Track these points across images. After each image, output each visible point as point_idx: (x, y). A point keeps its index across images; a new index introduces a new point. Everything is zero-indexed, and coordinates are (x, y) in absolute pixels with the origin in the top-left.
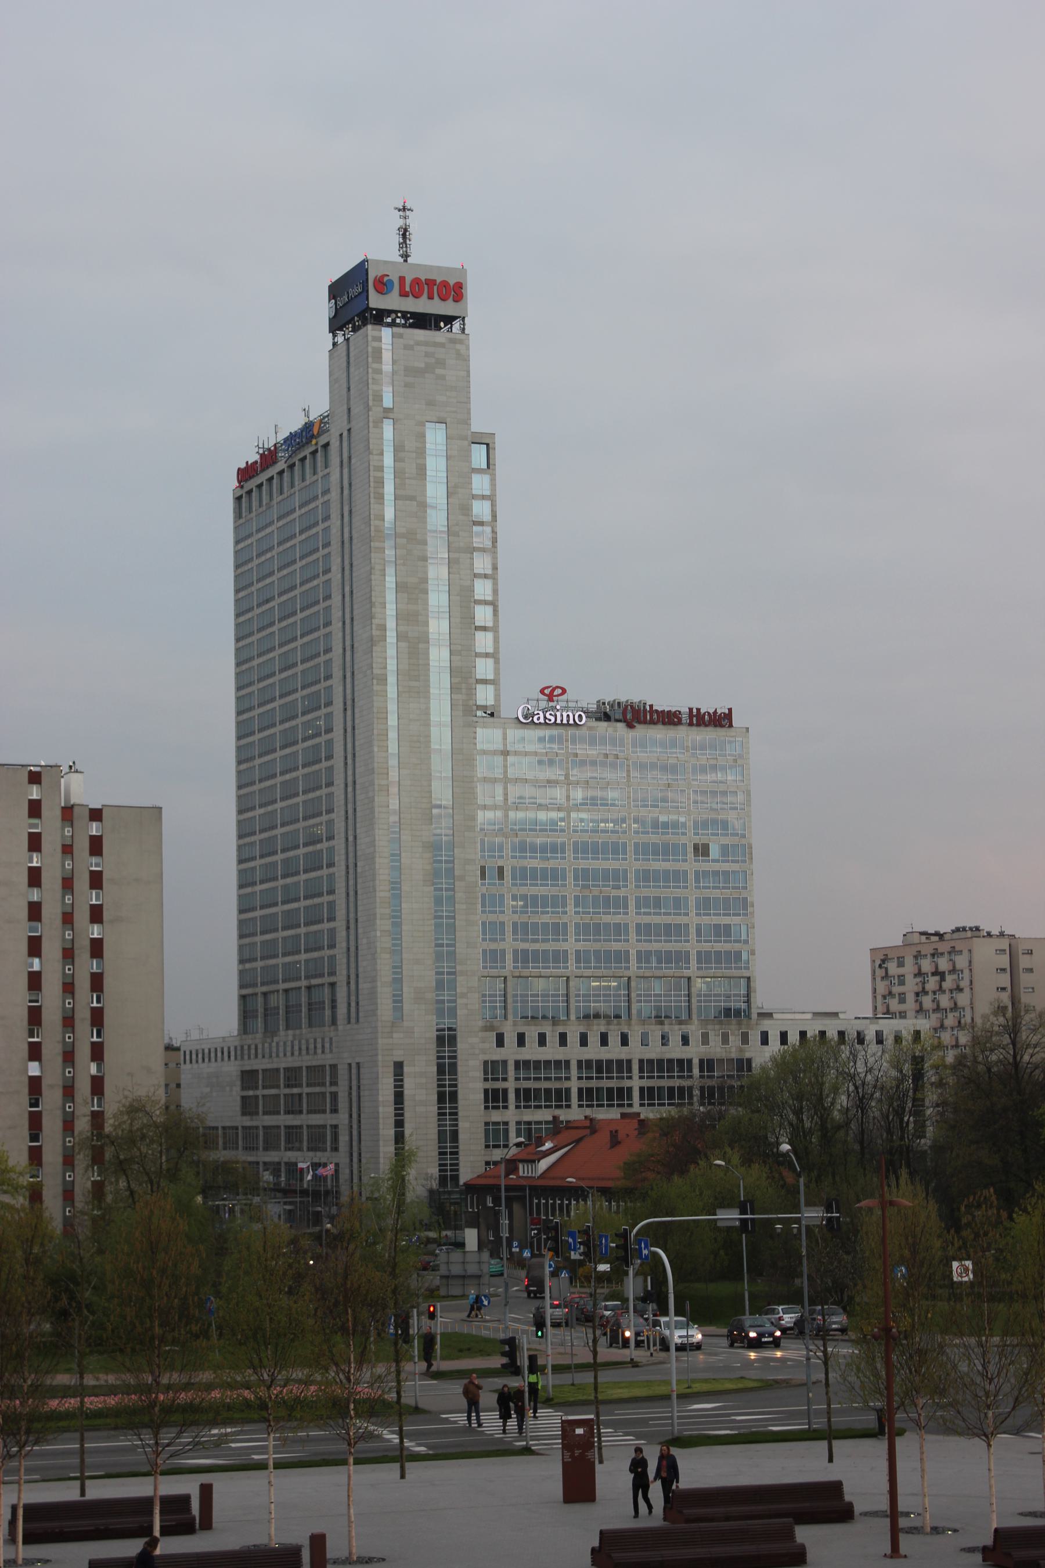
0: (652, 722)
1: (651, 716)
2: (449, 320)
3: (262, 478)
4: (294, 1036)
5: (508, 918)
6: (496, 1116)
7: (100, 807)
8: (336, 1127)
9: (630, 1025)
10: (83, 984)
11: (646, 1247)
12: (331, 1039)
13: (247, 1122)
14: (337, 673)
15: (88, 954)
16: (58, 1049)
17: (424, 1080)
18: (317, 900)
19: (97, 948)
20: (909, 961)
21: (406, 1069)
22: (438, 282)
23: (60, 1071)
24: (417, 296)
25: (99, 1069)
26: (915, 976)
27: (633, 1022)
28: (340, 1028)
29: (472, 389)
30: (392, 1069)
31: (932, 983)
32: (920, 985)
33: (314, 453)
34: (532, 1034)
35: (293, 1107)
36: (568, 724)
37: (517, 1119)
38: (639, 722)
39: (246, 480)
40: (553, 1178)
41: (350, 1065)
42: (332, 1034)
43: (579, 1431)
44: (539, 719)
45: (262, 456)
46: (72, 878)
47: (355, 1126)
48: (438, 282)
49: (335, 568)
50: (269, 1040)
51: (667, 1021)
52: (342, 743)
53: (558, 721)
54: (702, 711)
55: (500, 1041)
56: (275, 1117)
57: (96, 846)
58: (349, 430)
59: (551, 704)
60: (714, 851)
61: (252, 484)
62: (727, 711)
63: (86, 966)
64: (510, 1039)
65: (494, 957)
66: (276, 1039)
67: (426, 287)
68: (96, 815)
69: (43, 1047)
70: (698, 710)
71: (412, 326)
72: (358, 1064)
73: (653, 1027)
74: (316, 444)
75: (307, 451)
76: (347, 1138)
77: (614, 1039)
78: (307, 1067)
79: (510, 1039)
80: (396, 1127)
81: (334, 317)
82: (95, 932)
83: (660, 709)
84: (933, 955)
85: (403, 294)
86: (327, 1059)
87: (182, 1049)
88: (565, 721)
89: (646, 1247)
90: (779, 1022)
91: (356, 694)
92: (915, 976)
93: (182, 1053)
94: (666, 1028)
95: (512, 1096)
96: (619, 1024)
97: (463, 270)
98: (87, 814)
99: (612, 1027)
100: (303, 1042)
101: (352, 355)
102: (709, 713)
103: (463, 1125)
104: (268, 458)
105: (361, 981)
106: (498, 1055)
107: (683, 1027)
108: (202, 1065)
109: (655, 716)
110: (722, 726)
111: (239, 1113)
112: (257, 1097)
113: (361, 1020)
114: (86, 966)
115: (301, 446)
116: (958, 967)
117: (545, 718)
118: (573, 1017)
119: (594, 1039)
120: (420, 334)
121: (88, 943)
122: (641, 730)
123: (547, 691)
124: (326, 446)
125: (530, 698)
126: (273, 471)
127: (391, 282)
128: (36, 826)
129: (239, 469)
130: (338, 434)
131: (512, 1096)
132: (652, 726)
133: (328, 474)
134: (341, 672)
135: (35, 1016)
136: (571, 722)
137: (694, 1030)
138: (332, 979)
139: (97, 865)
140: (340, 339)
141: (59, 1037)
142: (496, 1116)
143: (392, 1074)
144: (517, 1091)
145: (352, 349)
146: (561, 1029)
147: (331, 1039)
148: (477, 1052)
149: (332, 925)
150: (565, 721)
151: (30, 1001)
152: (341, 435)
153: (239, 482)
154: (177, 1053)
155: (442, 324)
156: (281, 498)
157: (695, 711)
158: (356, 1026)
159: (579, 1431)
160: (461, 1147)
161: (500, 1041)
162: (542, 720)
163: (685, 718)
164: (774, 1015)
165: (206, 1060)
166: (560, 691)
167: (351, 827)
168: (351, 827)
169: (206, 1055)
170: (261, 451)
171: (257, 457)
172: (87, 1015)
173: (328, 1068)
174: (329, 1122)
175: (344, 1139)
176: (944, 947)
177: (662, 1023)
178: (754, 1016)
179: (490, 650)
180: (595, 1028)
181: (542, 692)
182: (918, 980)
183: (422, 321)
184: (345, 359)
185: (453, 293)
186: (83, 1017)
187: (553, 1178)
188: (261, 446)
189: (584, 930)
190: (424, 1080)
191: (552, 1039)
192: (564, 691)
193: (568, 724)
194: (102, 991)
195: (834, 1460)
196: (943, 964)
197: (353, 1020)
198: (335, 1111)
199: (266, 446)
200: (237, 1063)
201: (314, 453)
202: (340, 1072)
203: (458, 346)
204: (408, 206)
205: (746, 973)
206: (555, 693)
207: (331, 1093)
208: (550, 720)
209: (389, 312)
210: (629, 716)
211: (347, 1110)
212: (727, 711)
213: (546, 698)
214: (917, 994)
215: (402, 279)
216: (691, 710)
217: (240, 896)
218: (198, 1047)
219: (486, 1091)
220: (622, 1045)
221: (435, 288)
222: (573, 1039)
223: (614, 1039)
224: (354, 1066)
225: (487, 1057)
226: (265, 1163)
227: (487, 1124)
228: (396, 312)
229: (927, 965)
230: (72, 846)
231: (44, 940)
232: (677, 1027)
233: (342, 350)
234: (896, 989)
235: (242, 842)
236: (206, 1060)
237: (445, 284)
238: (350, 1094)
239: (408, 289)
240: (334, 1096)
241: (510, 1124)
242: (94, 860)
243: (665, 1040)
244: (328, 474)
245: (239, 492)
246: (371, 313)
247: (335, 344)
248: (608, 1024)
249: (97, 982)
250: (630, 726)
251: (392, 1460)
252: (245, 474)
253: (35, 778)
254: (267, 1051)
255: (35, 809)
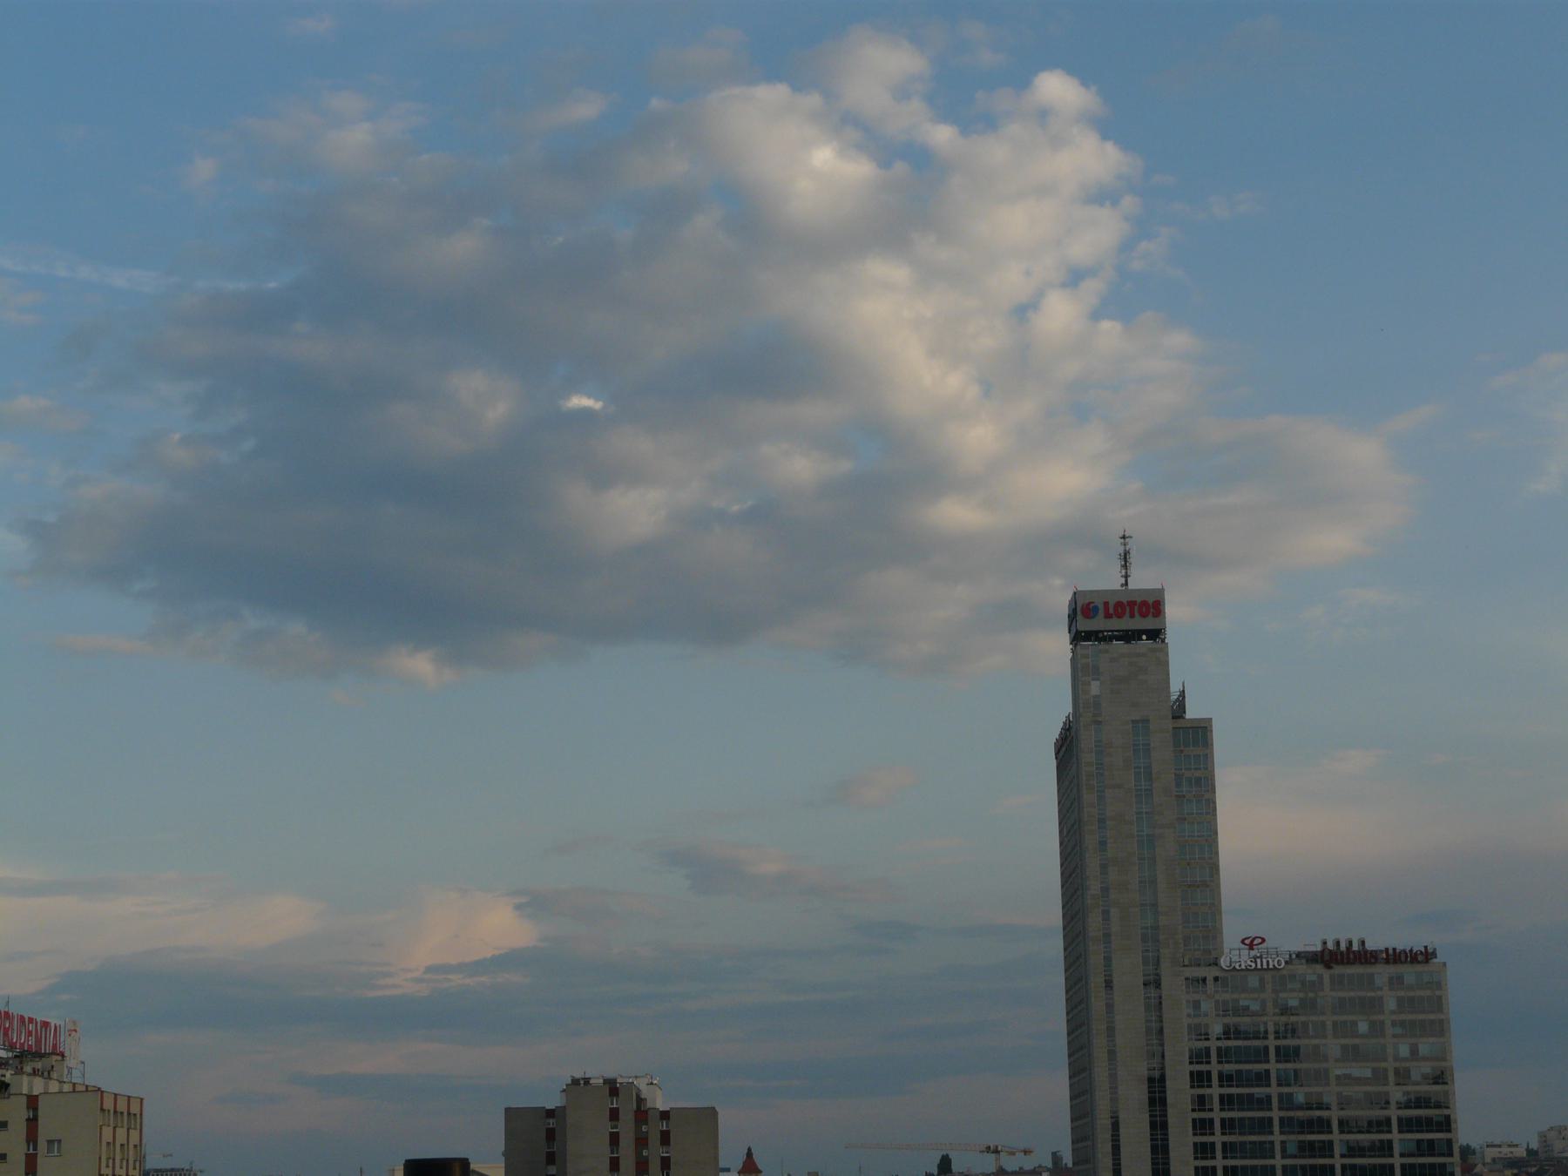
7: (668, 1109)
24: (1120, 616)
36: (1268, 969)
44: (1240, 966)
53: (1259, 966)
68: (665, 1115)
85: (1108, 616)
88: (1265, 966)
98: (658, 1114)
123: (1247, 942)
127: (1096, 608)
150: (1265, 966)
166: (1260, 940)
179: (77, 1090)
181: (1243, 942)
183: (1129, 636)
185: (1152, 610)
192: (1263, 940)
195: (727, 1166)
206: (1255, 942)
208: (1251, 966)
221: (1136, 608)
237: (1144, 603)
239: (1111, 611)
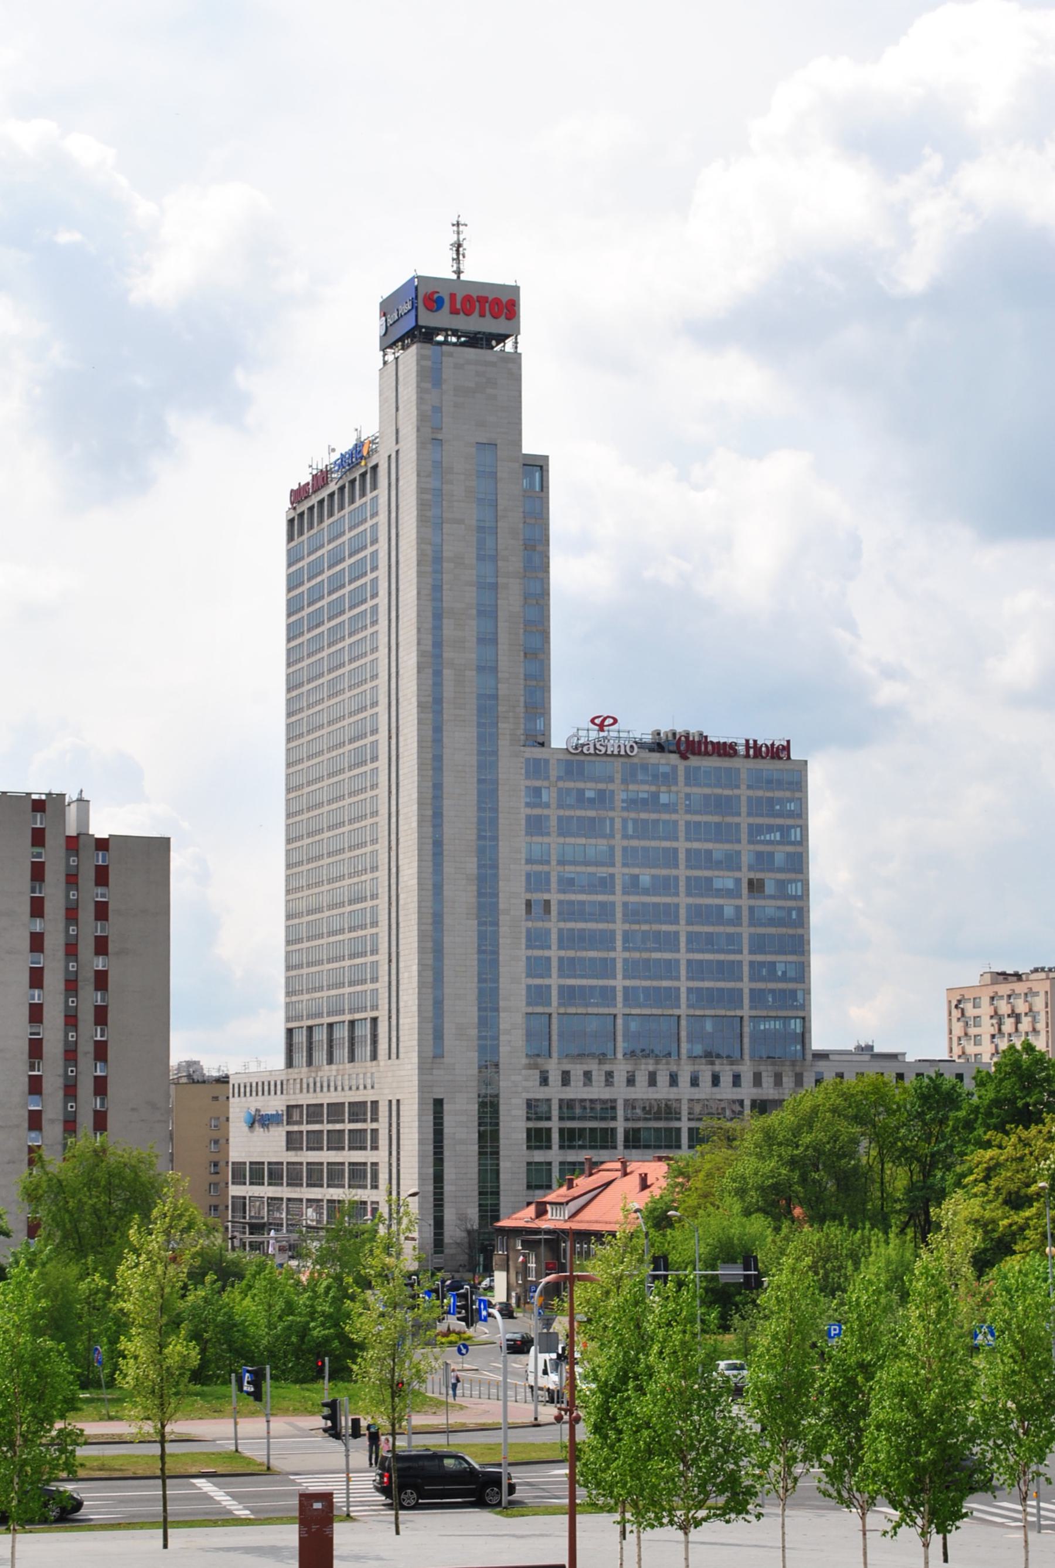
0: (707, 754)
1: (706, 748)
2: (502, 338)
3: (314, 500)
4: (338, 1070)
5: (554, 953)
6: (539, 1156)
8: (375, 1164)
9: (679, 1065)
10: (86, 1016)
11: (485, 1308)
12: (372, 1074)
13: (292, 1157)
14: (383, 700)
15: (92, 987)
16: (60, 1082)
17: (464, 1118)
18: (361, 933)
19: (101, 980)
20: (985, 1001)
21: (446, 1107)
22: (490, 299)
23: (60, 1105)
24: (468, 313)
25: (102, 1104)
26: (992, 1017)
27: (683, 1062)
28: (382, 1063)
29: (378, 421)
30: (431, 1107)
31: (1008, 1025)
32: (996, 1026)
33: (363, 475)
34: (577, 1071)
35: (335, 1141)
37: (561, 1159)
38: (694, 754)
39: (299, 502)
40: (581, 1222)
41: (390, 1101)
42: (374, 1070)
43: (317, 1506)
45: (315, 477)
46: (77, 908)
47: (394, 1164)
48: (490, 299)
49: (383, 592)
50: (313, 1075)
51: (717, 1061)
52: (387, 771)
54: (759, 743)
55: (544, 1081)
56: (339, 1153)
57: (102, 876)
58: (397, 452)
59: (602, 734)
60: (770, 888)
61: (304, 507)
62: (785, 744)
63: (89, 998)
64: (555, 1078)
65: (538, 995)
66: (320, 1074)
67: (477, 304)
69: (44, 1080)
70: (755, 741)
71: (462, 344)
72: (398, 1101)
73: (703, 1067)
74: (366, 465)
75: (357, 474)
76: (387, 1176)
77: (663, 1079)
78: (350, 1103)
79: (555, 1078)
80: (435, 1165)
81: (385, 334)
82: (100, 963)
83: (715, 740)
84: (1009, 996)
85: (454, 311)
86: (368, 1096)
87: (231, 1082)
89: (485, 1308)
90: (836, 1064)
91: (401, 722)
92: (992, 1017)
93: (231, 1086)
94: (717, 1068)
95: (555, 1136)
96: (668, 1063)
97: (516, 289)
99: (660, 1067)
100: (346, 1077)
101: (400, 374)
102: (766, 746)
103: (504, 1165)
104: (321, 479)
105: (401, 1015)
106: (541, 1093)
107: (734, 1067)
108: (250, 1099)
109: (710, 747)
110: (780, 758)
111: (285, 1148)
112: (301, 1132)
113: (401, 1055)
114: (89, 998)
115: (353, 466)
116: (1035, 1009)
117: (595, 748)
118: (620, 1056)
119: (642, 1079)
120: (471, 352)
121: (92, 975)
122: (694, 761)
123: (597, 721)
124: (375, 468)
125: (580, 726)
126: (324, 494)
128: (39, 855)
129: (292, 491)
130: (386, 455)
131: (555, 1136)
132: (706, 758)
133: (377, 496)
134: (387, 699)
135: (36, 1049)
136: (622, 753)
137: (746, 1070)
138: (374, 1014)
139: (103, 896)
140: (390, 358)
141: (61, 1071)
142: (539, 1156)
143: (431, 1112)
144: (561, 1131)
145: (400, 368)
146: (607, 1067)
147: (372, 1074)
148: (520, 1089)
149: (374, 958)
151: (31, 1034)
152: (389, 457)
153: (292, 503)
154: (225, 1085)
155: (494, 343)
156: (332, 520)
157: (751, 742)
158: (397, 1062)
159: (317, 1506)
160: (502, 1187)
161: (544, 1081)
162: (592, 751)
163: (742, 750)
164: (831, 1057)
165: (254, 1093)
166: (611, 721)
167: (393, 859)
168: (393, 859)
169: (254, 1089)
170: (315, 472)
171: (309, 479)
172: (91, 1048)
173: (369, 1104)
174: (370, 1160)
175: (383, 1176)
176: (1020, 988)
177: (712, 1063)
178: (809, 1057)
180: (643, 1067)
181: (593, 721)
182: (994, 1021)
184: (394, 378)
186: (86, 1049)
187: (581, 1222)
188: (314, 466)
189: (632, 969)
190: (464, 1118)
191: (598, 1077)
192: (615, 721)
193: (619, 755)
194: (106, 1024)
196: (1021, 1007)
197: (394, 1056)
198: (375, 1148)
199: (320, 467)
200: (284, 1097)
201: (363, 475)
202: (381, 1109)
203: (510, 366)
204: (462, 221)
205: (801, 1014)
206: (606, 723)
207: (372, 1130)
209: (438, 331)
210: (682, 748)
211: (387, 1147)
212: (785, 744)
213: (597, 728)
214: (993, 1036)
215: (453, 296)
216: (747, 741)
217: (287, 927)
218: (246, 1080)
219: (529, 1130)
220: (671, 1085)
221: (487, 305)
222: (620, 1078)
223: (663, 1079)
224: (394, 1103)
225: (531, 1096)
226: (308, 1200)
227: (529, 1164)
228: (446, 330)
229: (1004, 1008)
230: (76, 875)
231: (46, 972)
232: (728, 1068)
233: (391, 367)
234: (972, 1031)
235: (290, 872)
236: (254, 1093)
237: (497, 301)
238: (390, 1131)
239: (458, 306)
240: (375, 1132)
241: (553, 1164)
242: (100, 890)
243: (716, 1081)
244: (377, 496)
245: (292, 514)
246: (420, 331)
247: (385, 363)
248: (657, 1063)
249: (101, 1016)
250: (684, 757)
251: (152, 1525)
252: (298, 495)
253: (39, 806)
254: (339, 1083)
255: (38, 838)
